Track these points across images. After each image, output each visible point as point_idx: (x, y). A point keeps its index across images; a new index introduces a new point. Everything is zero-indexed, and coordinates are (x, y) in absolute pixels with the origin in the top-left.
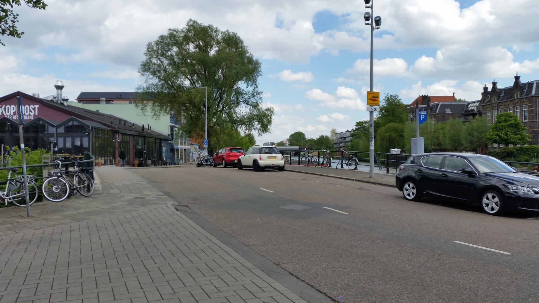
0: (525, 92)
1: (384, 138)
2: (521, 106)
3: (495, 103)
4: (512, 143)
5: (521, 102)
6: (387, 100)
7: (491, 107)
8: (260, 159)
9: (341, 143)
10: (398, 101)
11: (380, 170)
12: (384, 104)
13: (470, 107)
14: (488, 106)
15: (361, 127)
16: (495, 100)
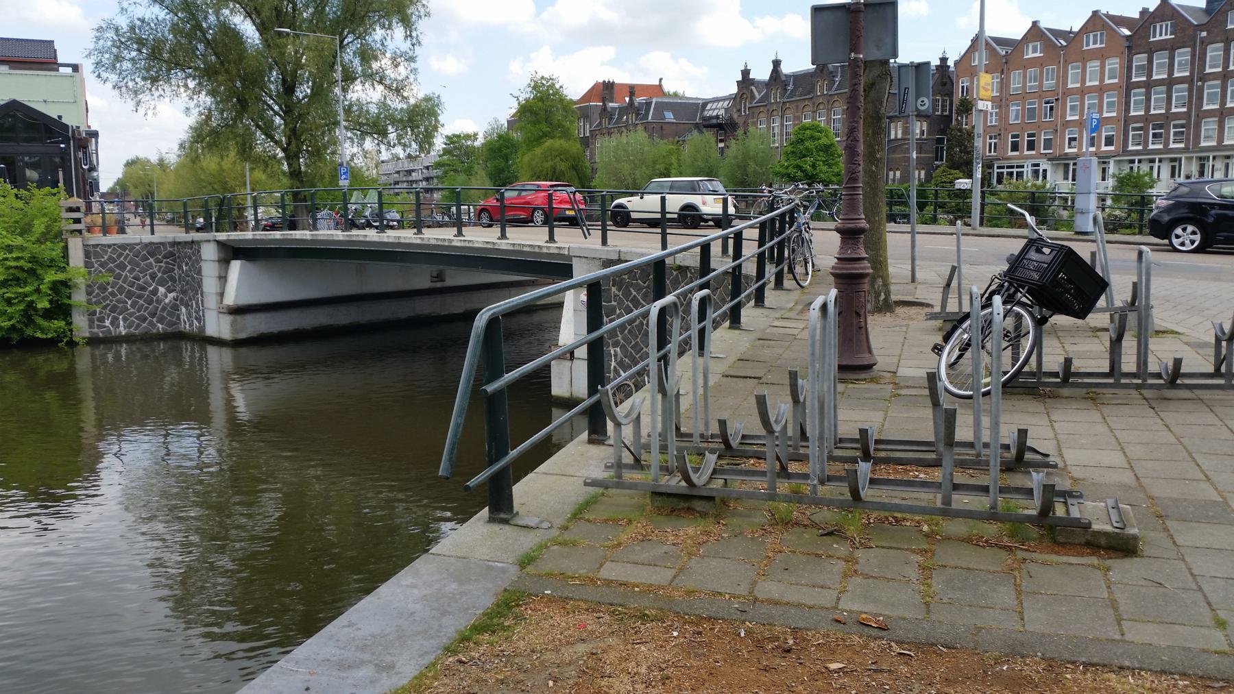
0: (837, 83)
1: (541, 171)
2: (829, 110)
3: (776, 102)
4: (822, 181)
5: (828, 101)
6: (534, 88)
7: (768, 110)
8: (704, 203)
9: (397, 183)
10: (557, 92)
11: (586, 238)
12: (528, 96)
13: (711, 109)
14: (762, 109)
15: (455, 148)
16: (776, 96)
